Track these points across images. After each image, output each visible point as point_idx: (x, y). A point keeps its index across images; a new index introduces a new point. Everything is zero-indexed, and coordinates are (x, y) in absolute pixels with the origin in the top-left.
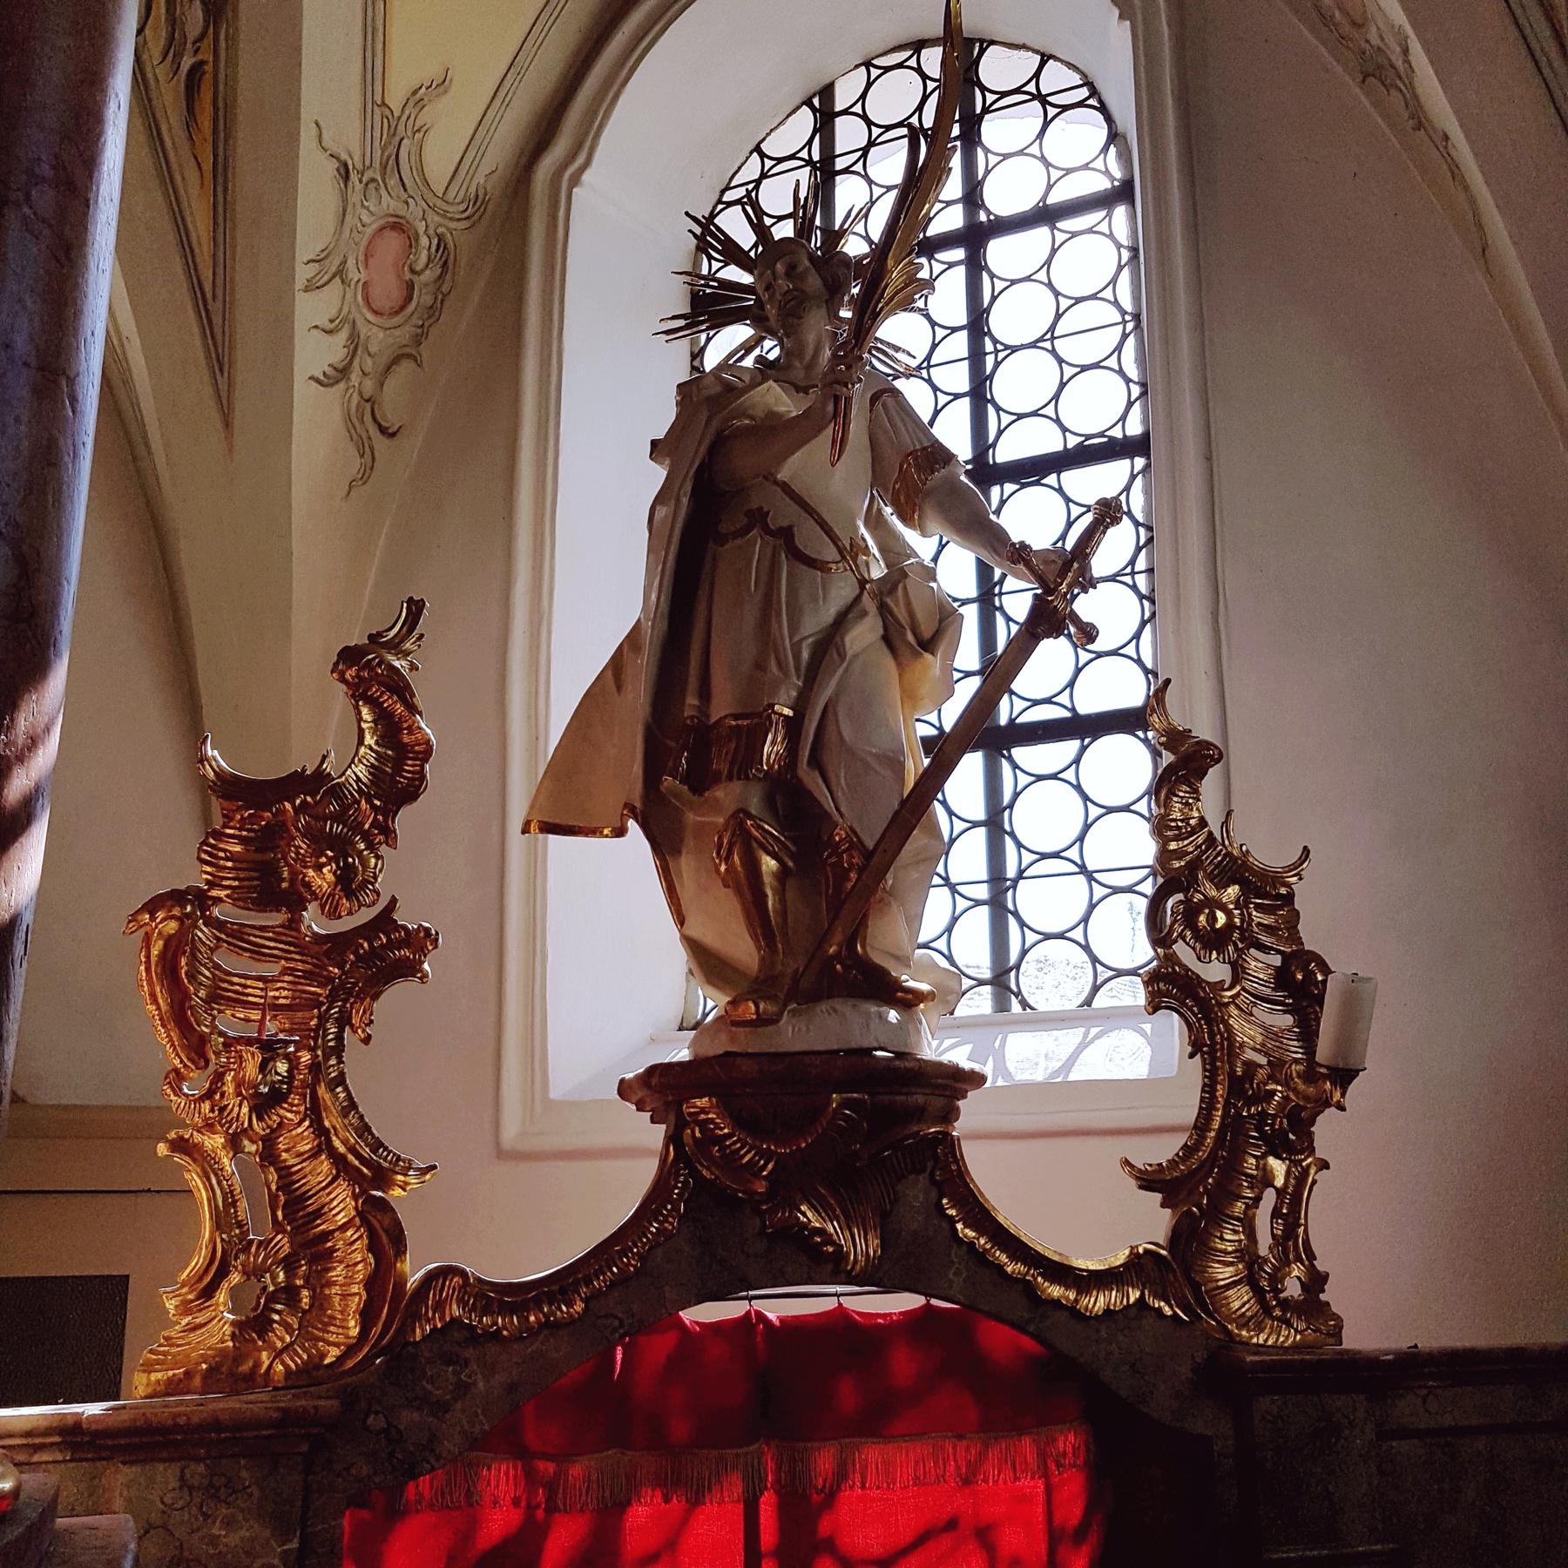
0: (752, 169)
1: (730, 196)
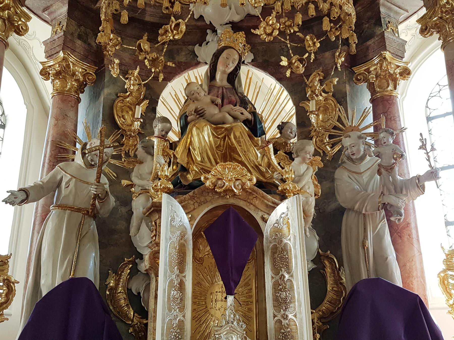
0: (438, 88)
1: (431, 95)
